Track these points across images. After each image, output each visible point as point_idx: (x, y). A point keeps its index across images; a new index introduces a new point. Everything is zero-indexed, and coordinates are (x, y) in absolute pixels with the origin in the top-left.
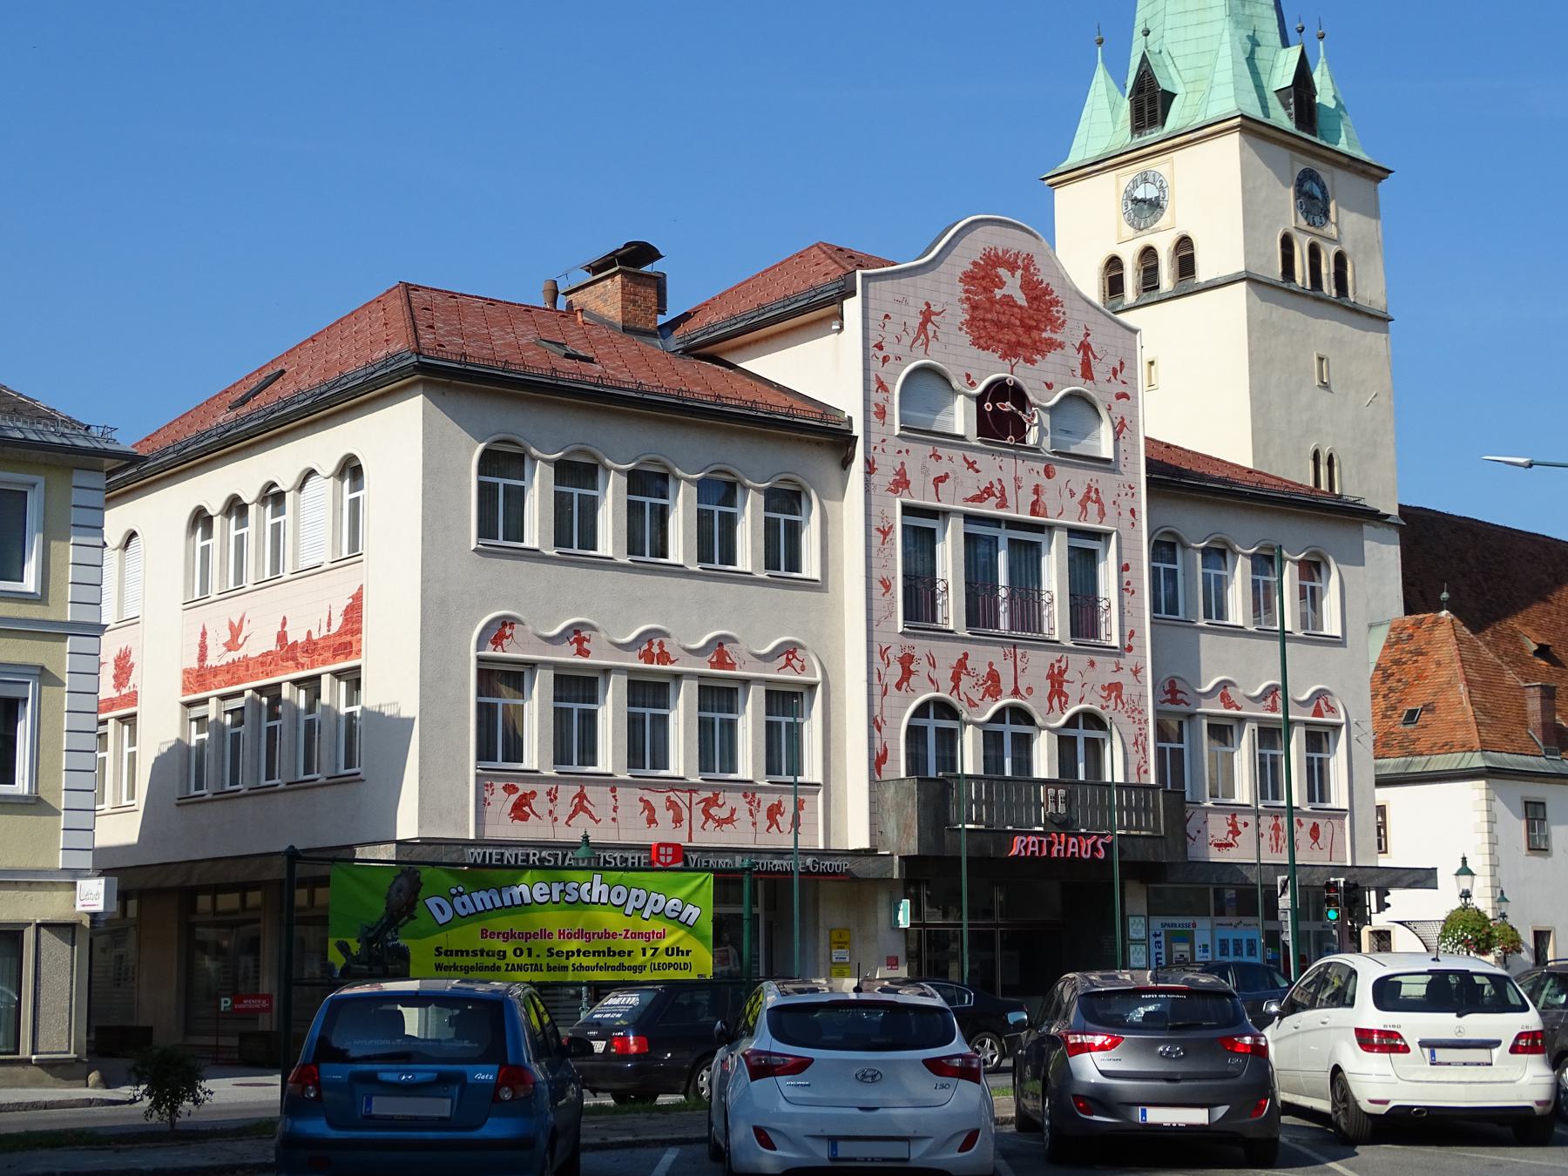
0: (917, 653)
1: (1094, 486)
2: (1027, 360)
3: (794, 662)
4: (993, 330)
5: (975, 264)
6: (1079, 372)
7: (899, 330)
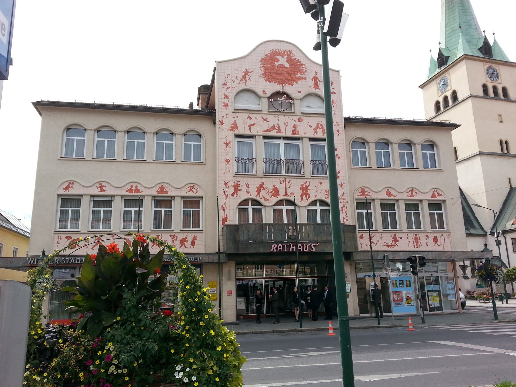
0: (241, 183)
1: (320, 123)
2: (289, 84)
3: (193, 190)
4: (274, 76)
5: (266, 55)
6: (313, 86)
7: (234, 79)
